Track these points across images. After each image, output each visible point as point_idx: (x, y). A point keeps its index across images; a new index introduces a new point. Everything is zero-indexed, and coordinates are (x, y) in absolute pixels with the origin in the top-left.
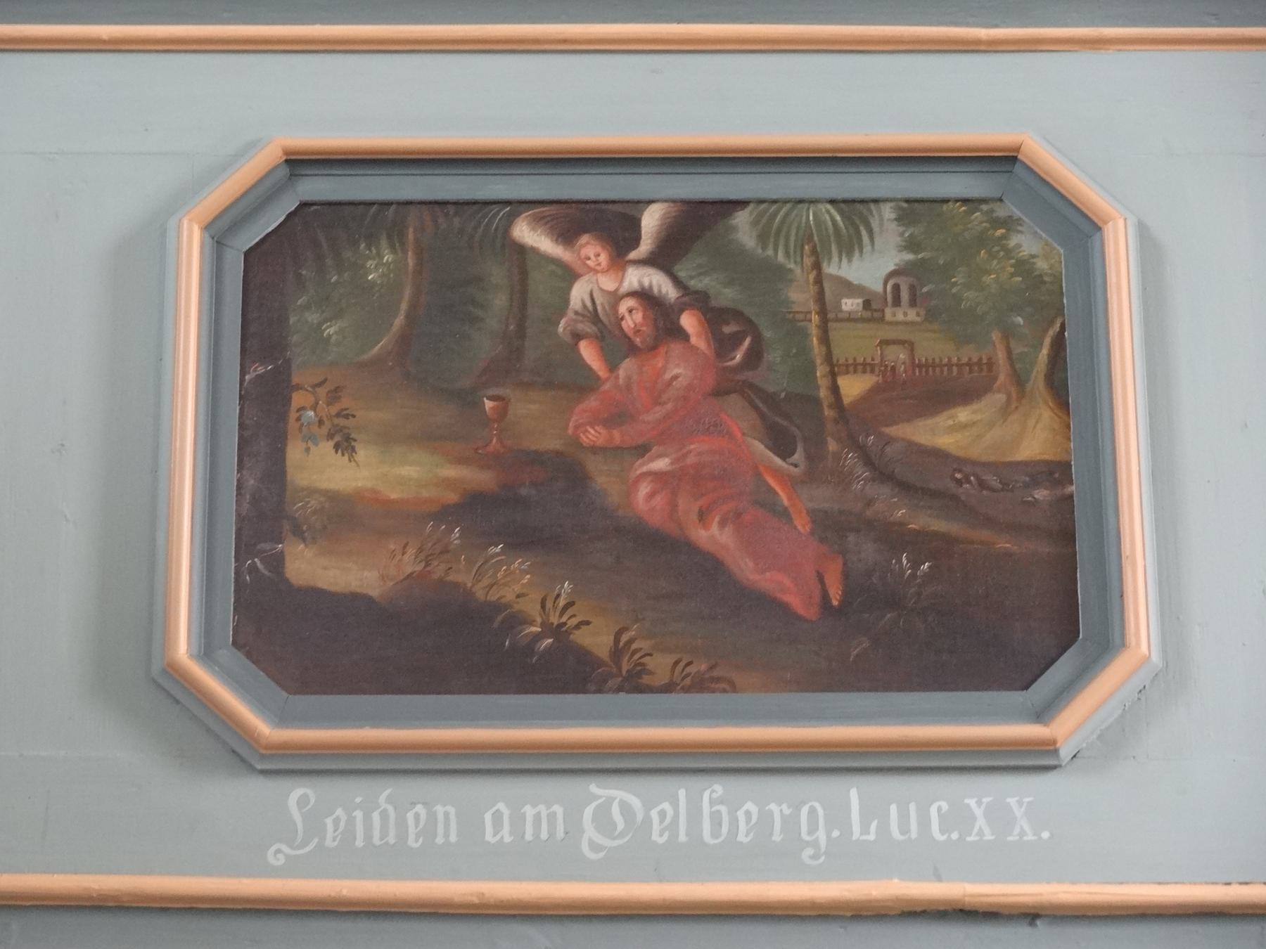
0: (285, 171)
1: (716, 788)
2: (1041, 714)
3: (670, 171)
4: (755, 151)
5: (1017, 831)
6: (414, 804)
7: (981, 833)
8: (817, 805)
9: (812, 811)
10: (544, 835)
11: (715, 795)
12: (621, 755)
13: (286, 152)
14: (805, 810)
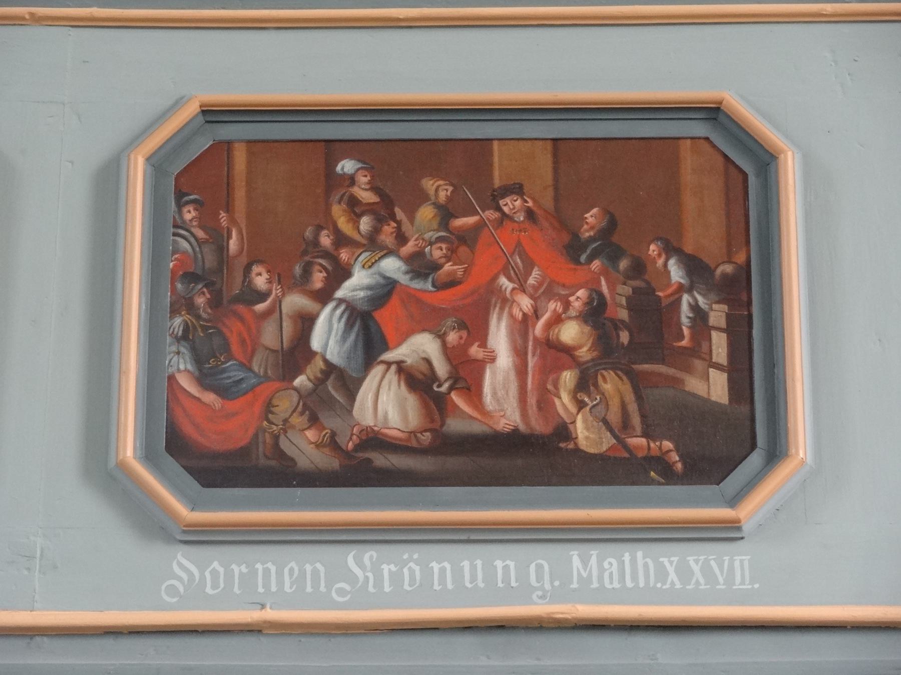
0: (201, 119)
5: (694, 581)
8: (318, 565)
12: (314, 531)
14: (533, 567)
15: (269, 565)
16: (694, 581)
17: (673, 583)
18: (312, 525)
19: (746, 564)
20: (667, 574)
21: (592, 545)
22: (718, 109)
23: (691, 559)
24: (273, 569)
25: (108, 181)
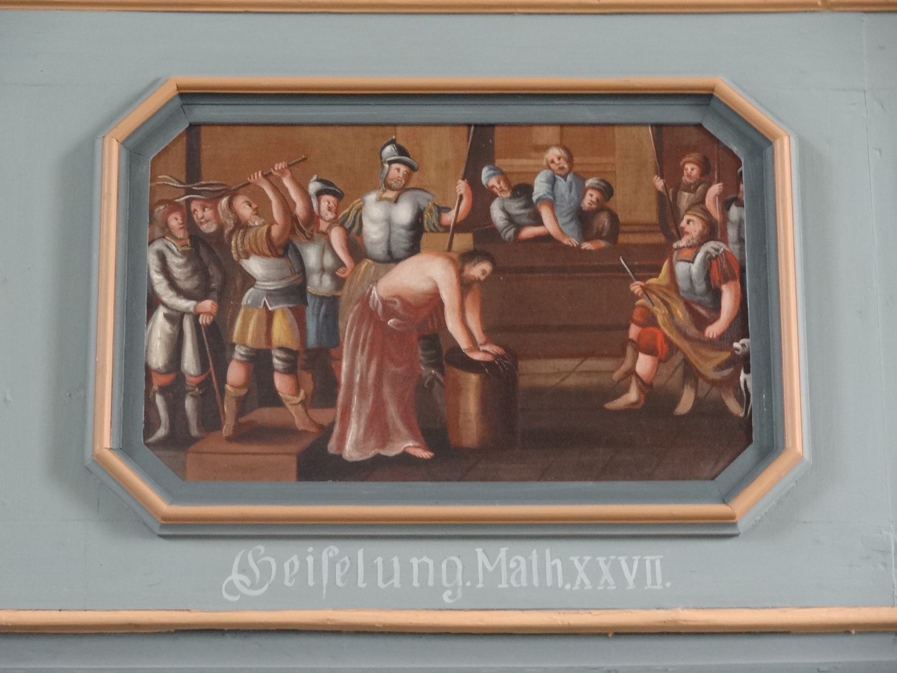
0: (178, 101)
4: (535, 89)
10: (549, 584)
11: (331, 555)
13: (178, 88)
15: (425, 559)
16: (602, 582)
18: (377, 519)
19: (658, 563)
20: (575, 572)
23: (601, 560)
24: (431, 562)
25: (79, 165)
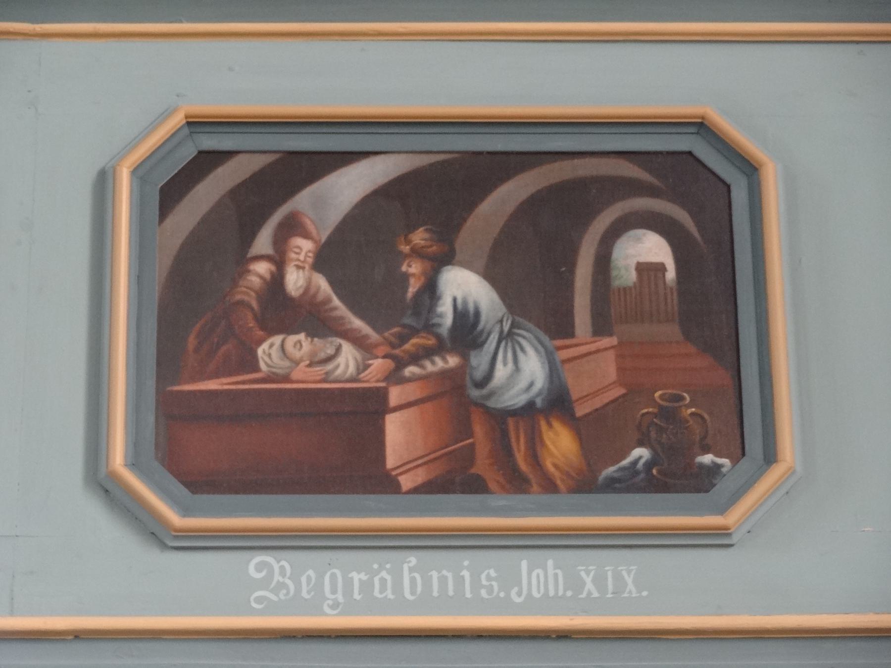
0: (186, 131)
1: (466, 559)
2: (722, 510)
3: (365, 131)
6: (490, 568)
7: (630, 592)
9: (333, 576)
10: (435, 594)
13: (186, 117)
16: (627, 590)
17: (590, 593)
21: (525, 553)
22: (702, 124)
